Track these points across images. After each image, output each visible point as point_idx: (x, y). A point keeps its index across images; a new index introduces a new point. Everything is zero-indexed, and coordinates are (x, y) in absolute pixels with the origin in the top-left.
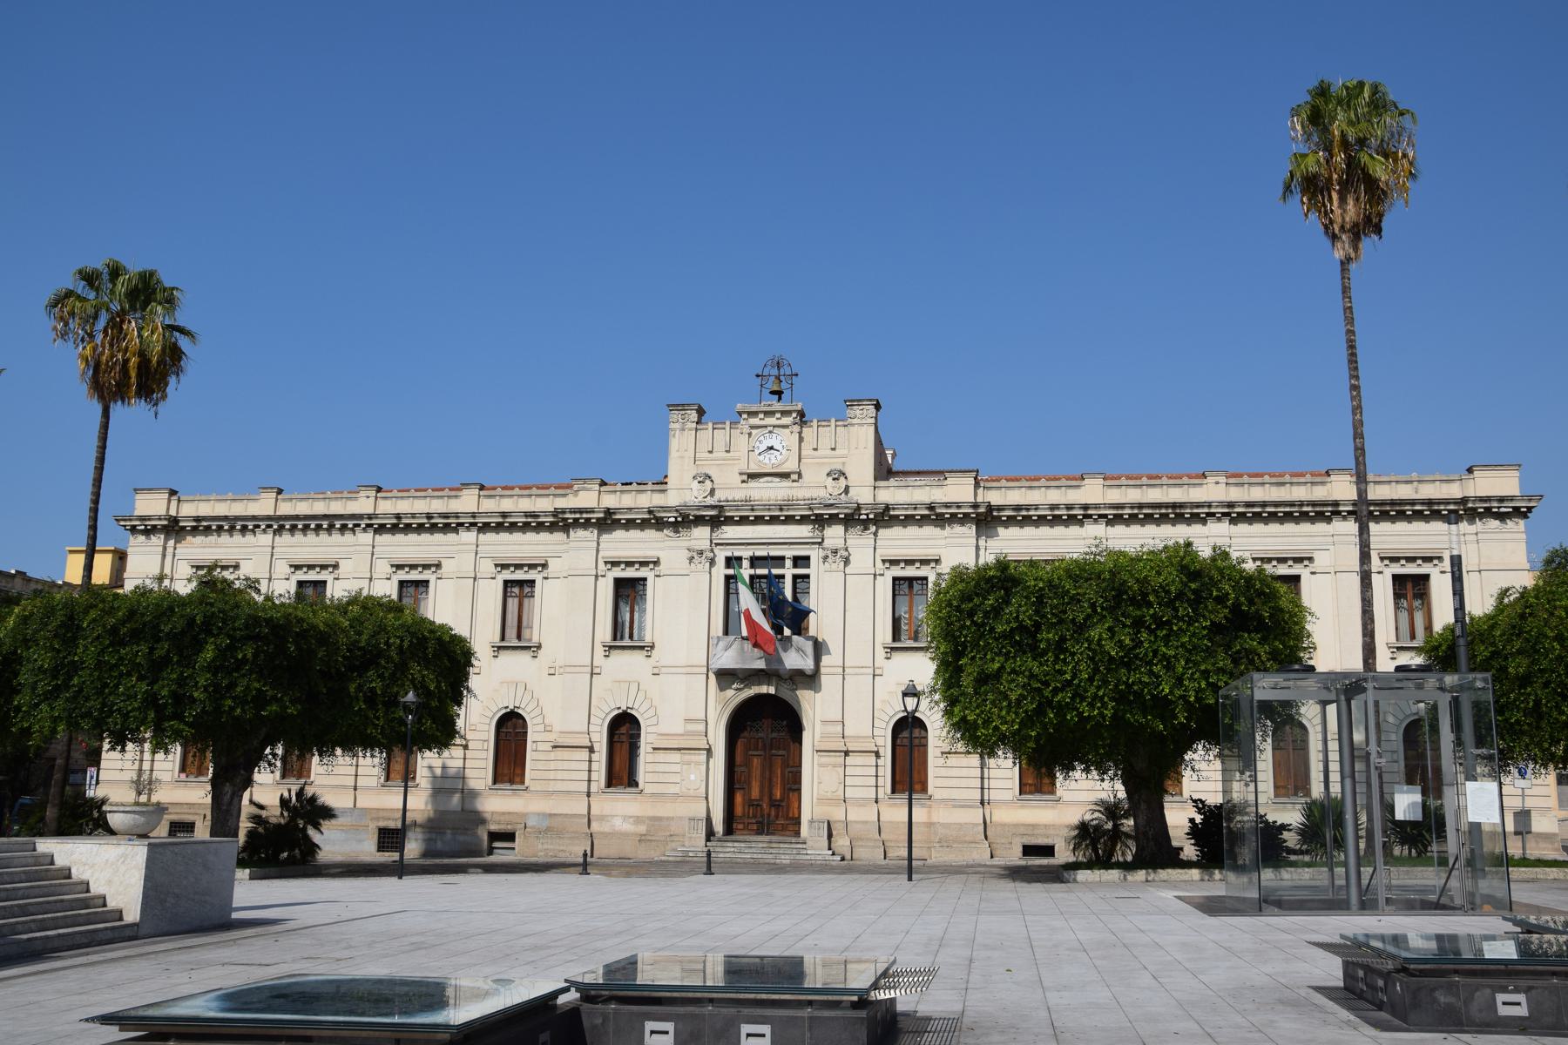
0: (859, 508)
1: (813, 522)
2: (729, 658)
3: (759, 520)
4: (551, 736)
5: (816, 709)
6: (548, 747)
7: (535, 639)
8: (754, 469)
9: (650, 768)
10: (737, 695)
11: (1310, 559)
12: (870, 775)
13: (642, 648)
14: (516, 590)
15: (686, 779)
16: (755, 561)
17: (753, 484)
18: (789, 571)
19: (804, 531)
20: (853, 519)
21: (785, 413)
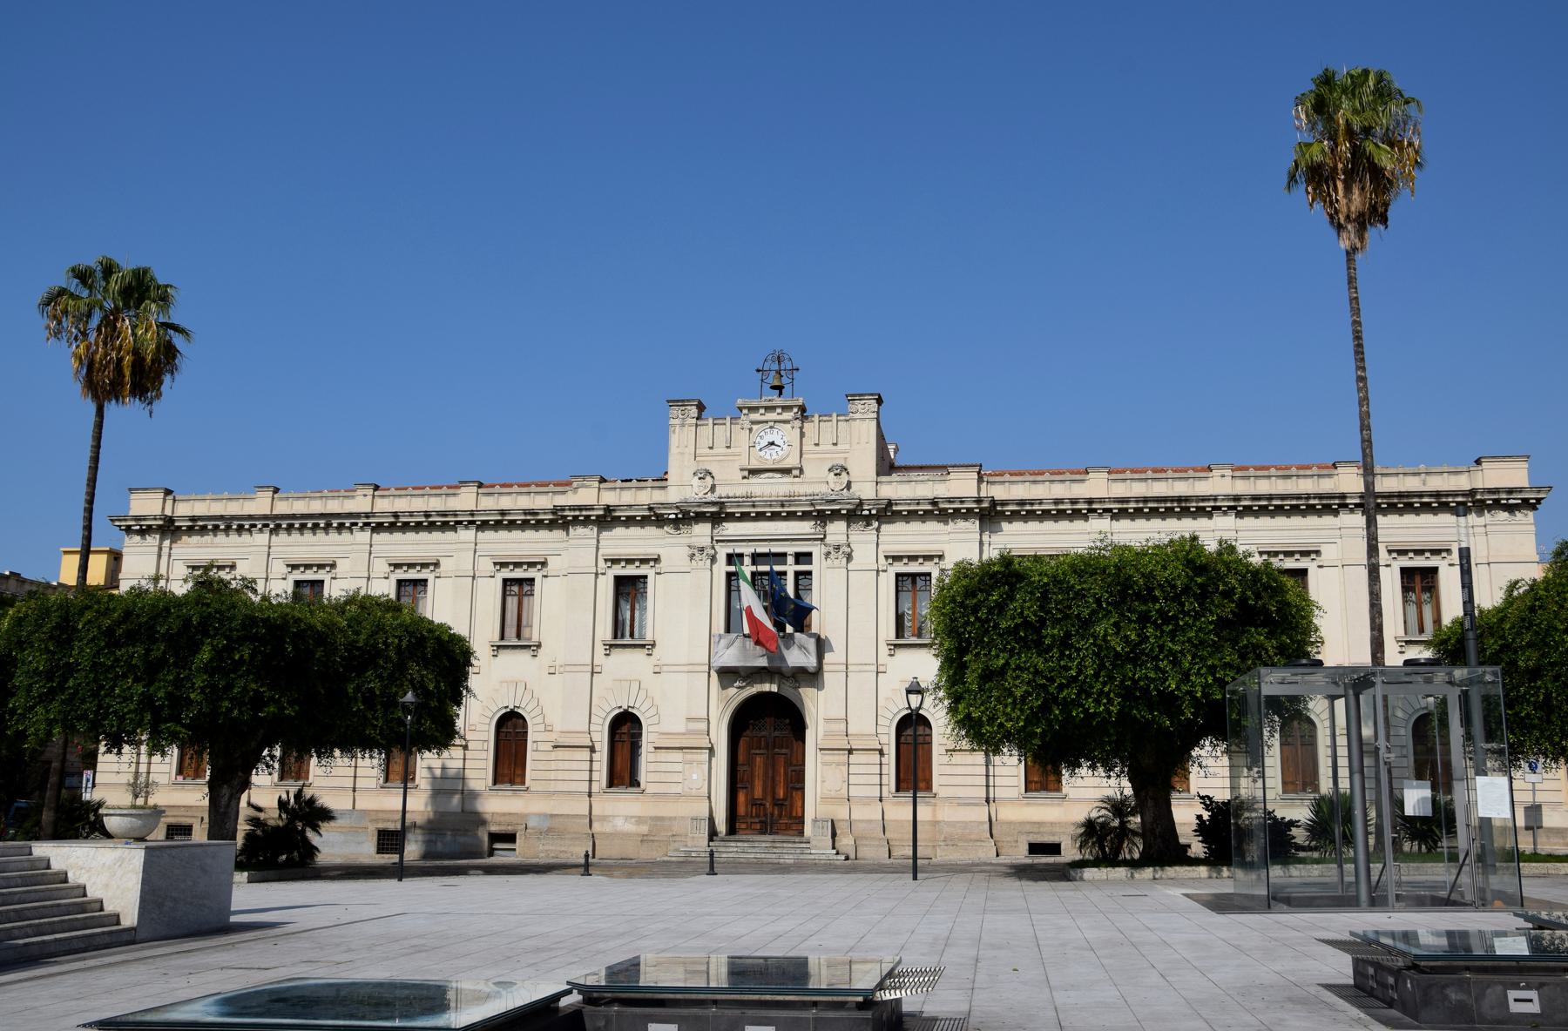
0: (861, 503)
2: (731, 656)
3: (760, 517)
4: (552, 737)
5: (819, 707)
6: (549, 747)
7: (535, 638)
8: (755, 465)
9: (652, 767)
10: (738, 694)
11: (1318, 553)
12: (874, 773)
13: (643, 646)
14: (515, 589)
15: (689, 778)
16: (756, 558)
17: (753, 480)
18: (790, 568)
19: (806, 527)
20: (855, 515)
21: (785, 408)
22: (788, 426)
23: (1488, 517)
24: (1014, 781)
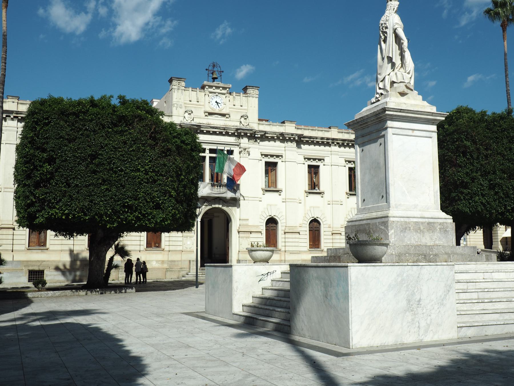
1: (236, 136)
3: (214, 133)
8: (210, 111)
11: (282, 156)
13: (278, 191)
16: (212, 151)
17: (210, 117)
19: (232, 140)
20: (253, 136)
21: (224, 88)
22: (224, 96)
23: (286, 144)
24: (23, 242)
